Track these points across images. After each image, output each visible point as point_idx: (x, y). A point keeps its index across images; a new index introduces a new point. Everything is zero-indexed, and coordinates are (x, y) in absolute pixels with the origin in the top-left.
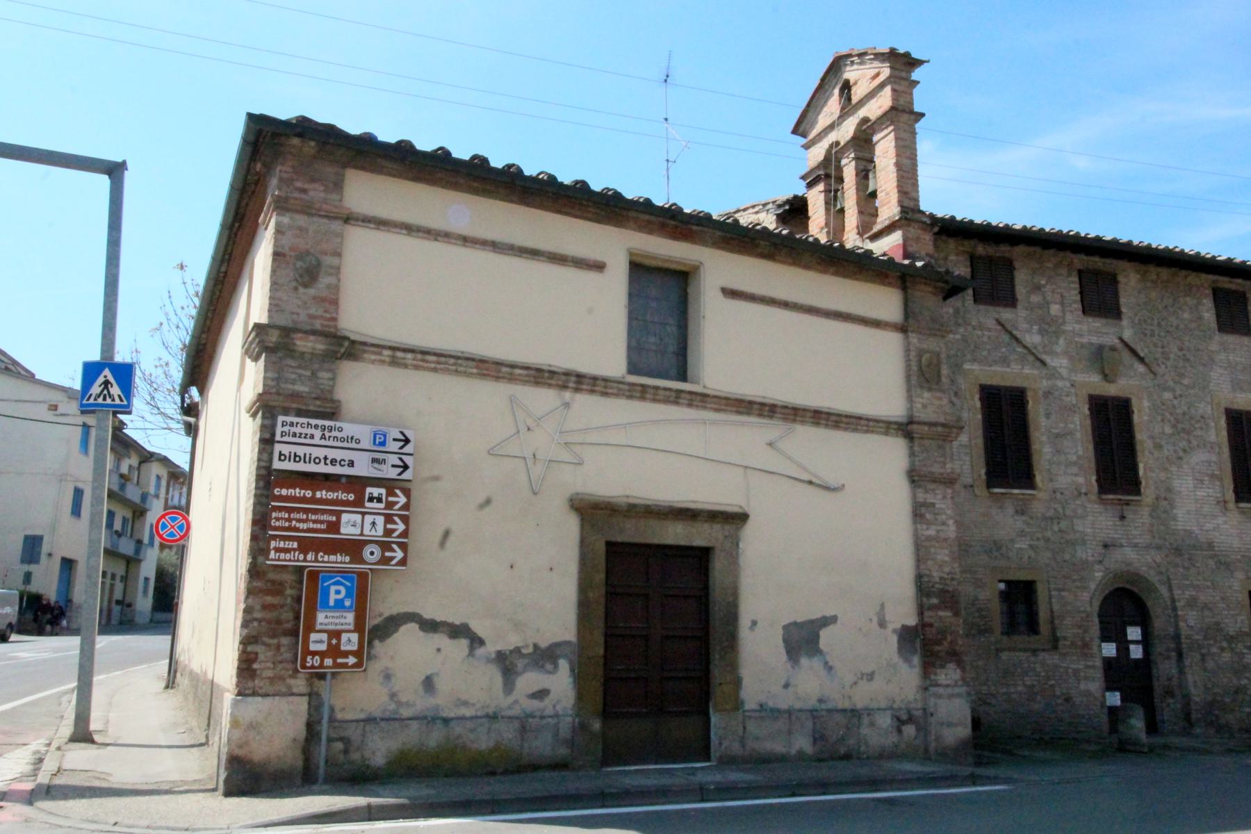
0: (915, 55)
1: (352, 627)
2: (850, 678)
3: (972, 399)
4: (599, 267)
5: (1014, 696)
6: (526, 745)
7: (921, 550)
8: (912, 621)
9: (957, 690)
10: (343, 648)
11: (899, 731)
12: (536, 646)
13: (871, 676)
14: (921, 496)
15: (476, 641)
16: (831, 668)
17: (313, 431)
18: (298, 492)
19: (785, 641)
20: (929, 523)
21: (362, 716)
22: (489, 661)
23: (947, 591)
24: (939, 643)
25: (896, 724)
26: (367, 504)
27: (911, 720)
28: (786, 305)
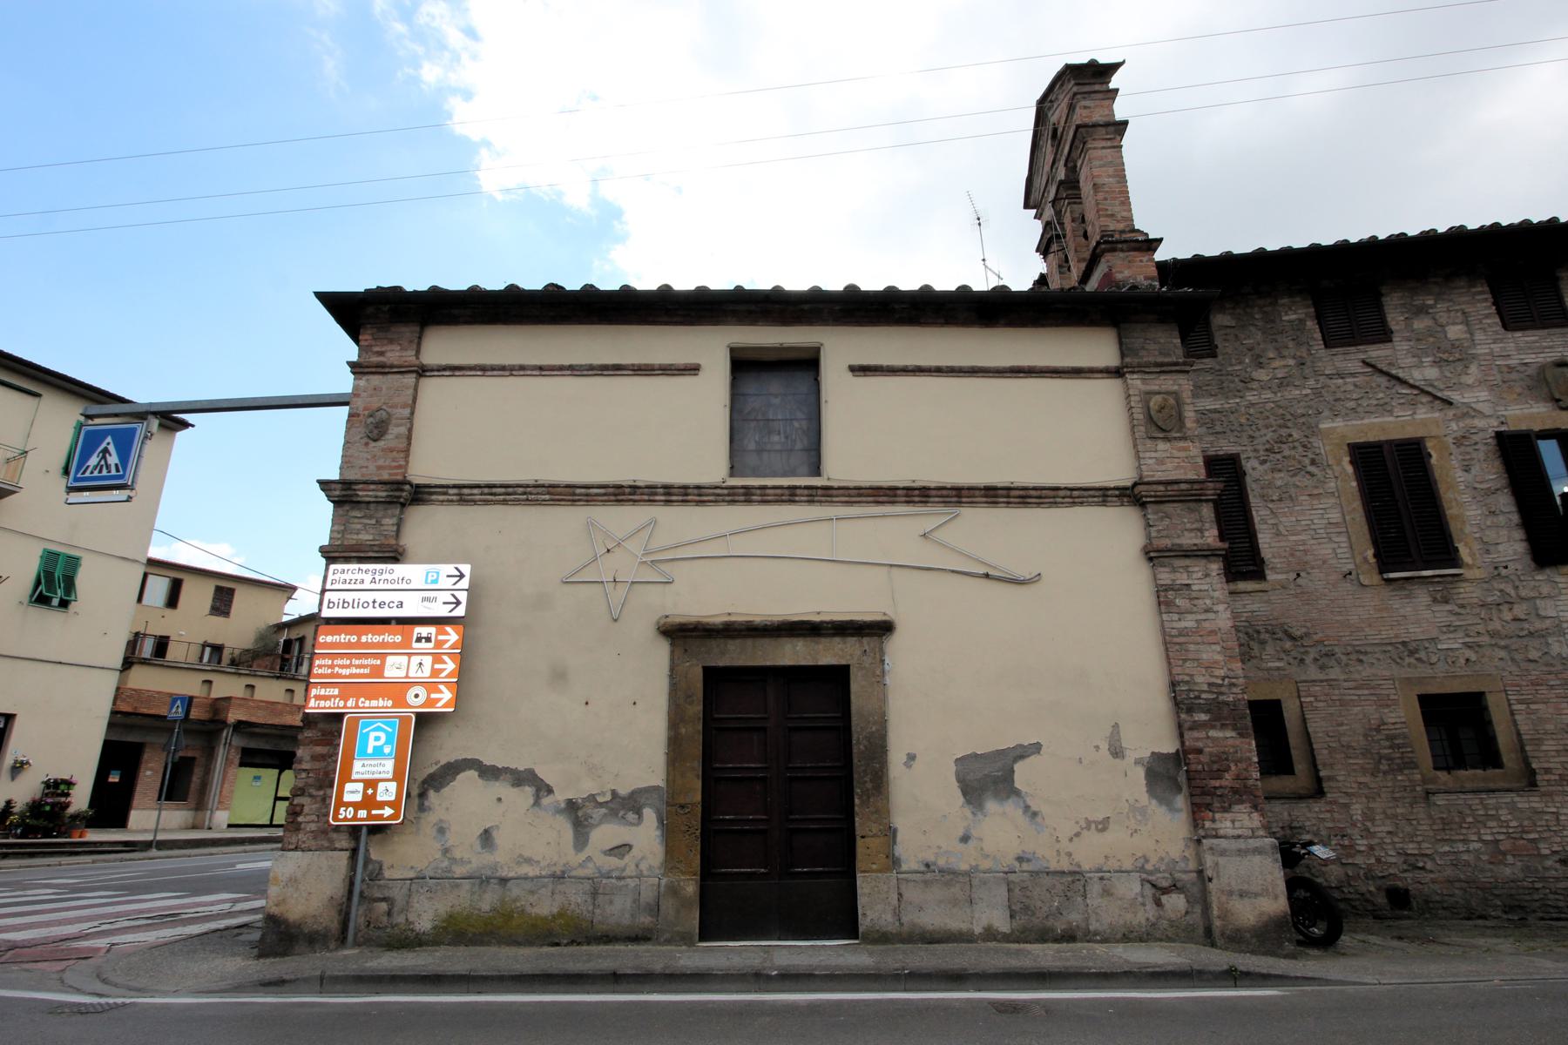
0: (1103, 59)
1: (390, 776)
2: (1067, 829)
3: (1339, 463)
4: (693, 370)
5: (1465, 857)
6: (598, 911)
7: (1172, 646)
8: (1169, 746)
9: (1253, 843)
10: (379, 798)
11: (1158, 903)
12: (614, 793)
13: (1103, 826)
14: (1165, 577)
15: (544, 790)
16: (1035, 814)
17: (363, 576)
18: (343, 638)
20: (1182, 613)
21: (412, 874)
22: (559, 811)
24: (1218, 774)
25: (1149, 891)
26: (415, 645)
27: (1175, 887)
28: (938, 371)
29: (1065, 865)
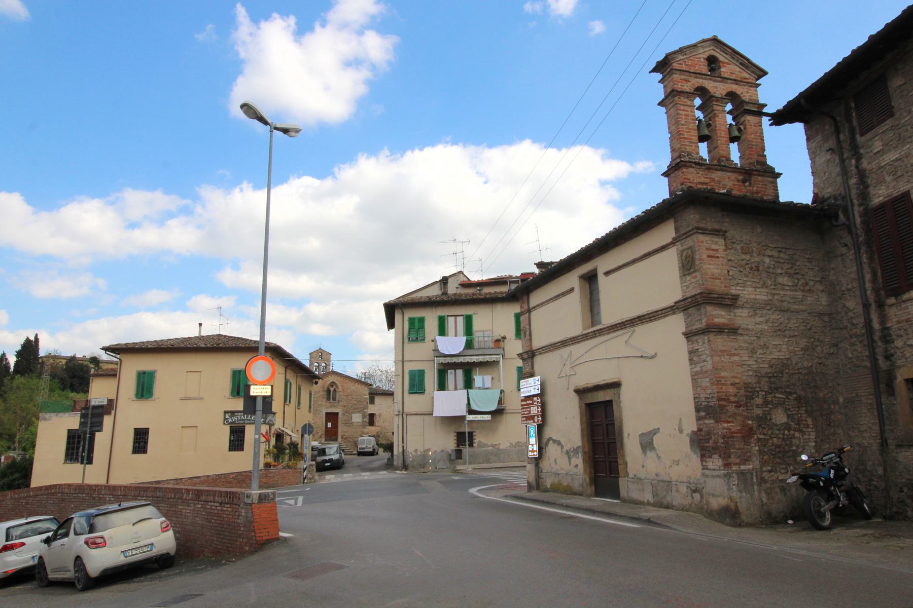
7: (695, 378)
9: (717, 473)
13: (677, 463)
19: (641, 444)
23: (711, 406)
24: (708, 441)
25: (690, 492)
28: (634, 261)
29: (667, 479)
